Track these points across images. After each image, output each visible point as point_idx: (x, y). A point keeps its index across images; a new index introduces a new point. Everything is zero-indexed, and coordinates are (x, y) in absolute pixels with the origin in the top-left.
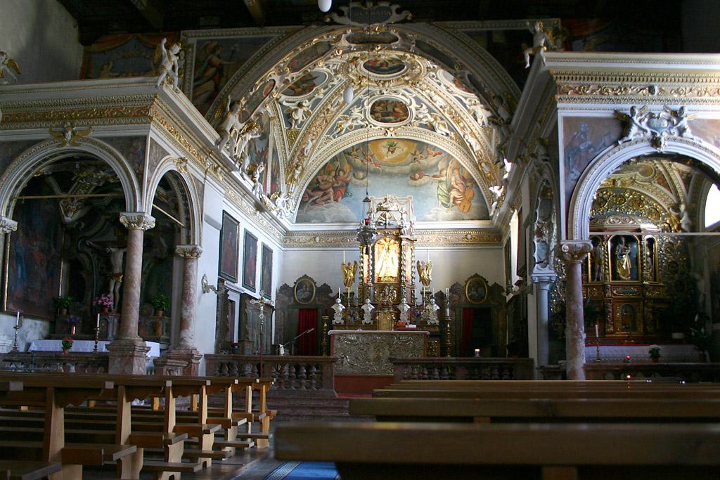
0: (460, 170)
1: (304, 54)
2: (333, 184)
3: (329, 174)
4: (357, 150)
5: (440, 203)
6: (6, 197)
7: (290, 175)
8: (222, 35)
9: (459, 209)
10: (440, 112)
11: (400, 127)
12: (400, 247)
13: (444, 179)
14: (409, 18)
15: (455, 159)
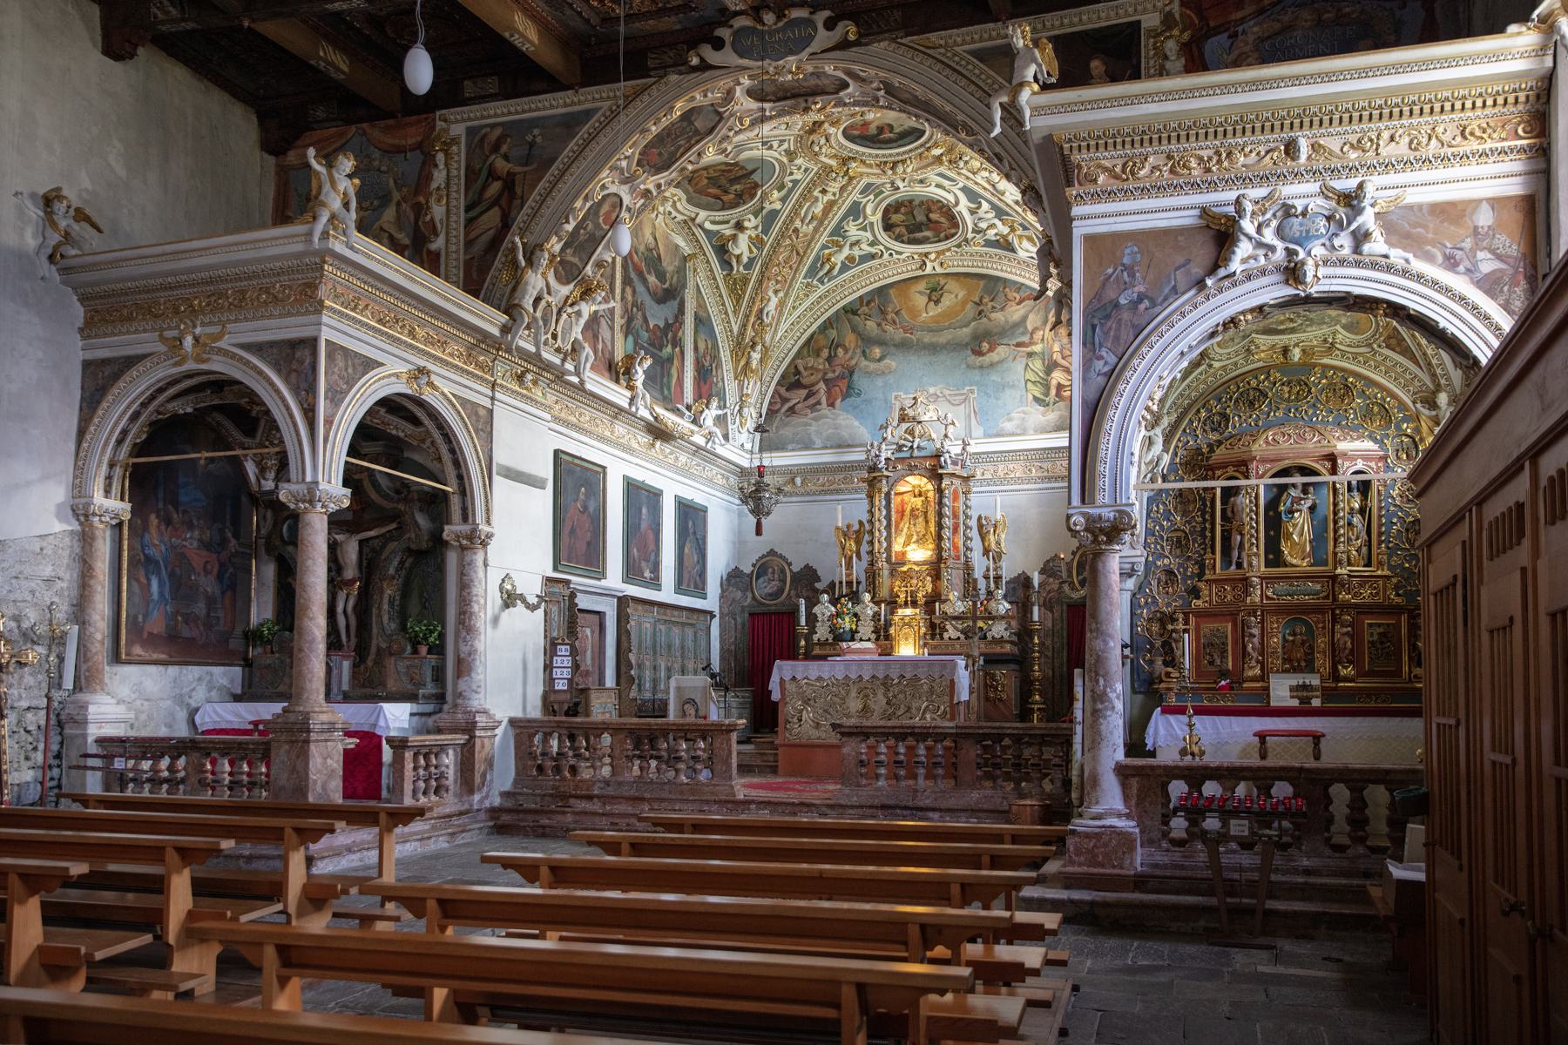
1: (669, 135)
2: (825, 374)
3: (818, 356)
5: (1031, 397)
6: (100, 462)
7: (742, 363)
8: (510, 113)
11: (949, 249)
13: (1038, 348)
14: (852, 37)
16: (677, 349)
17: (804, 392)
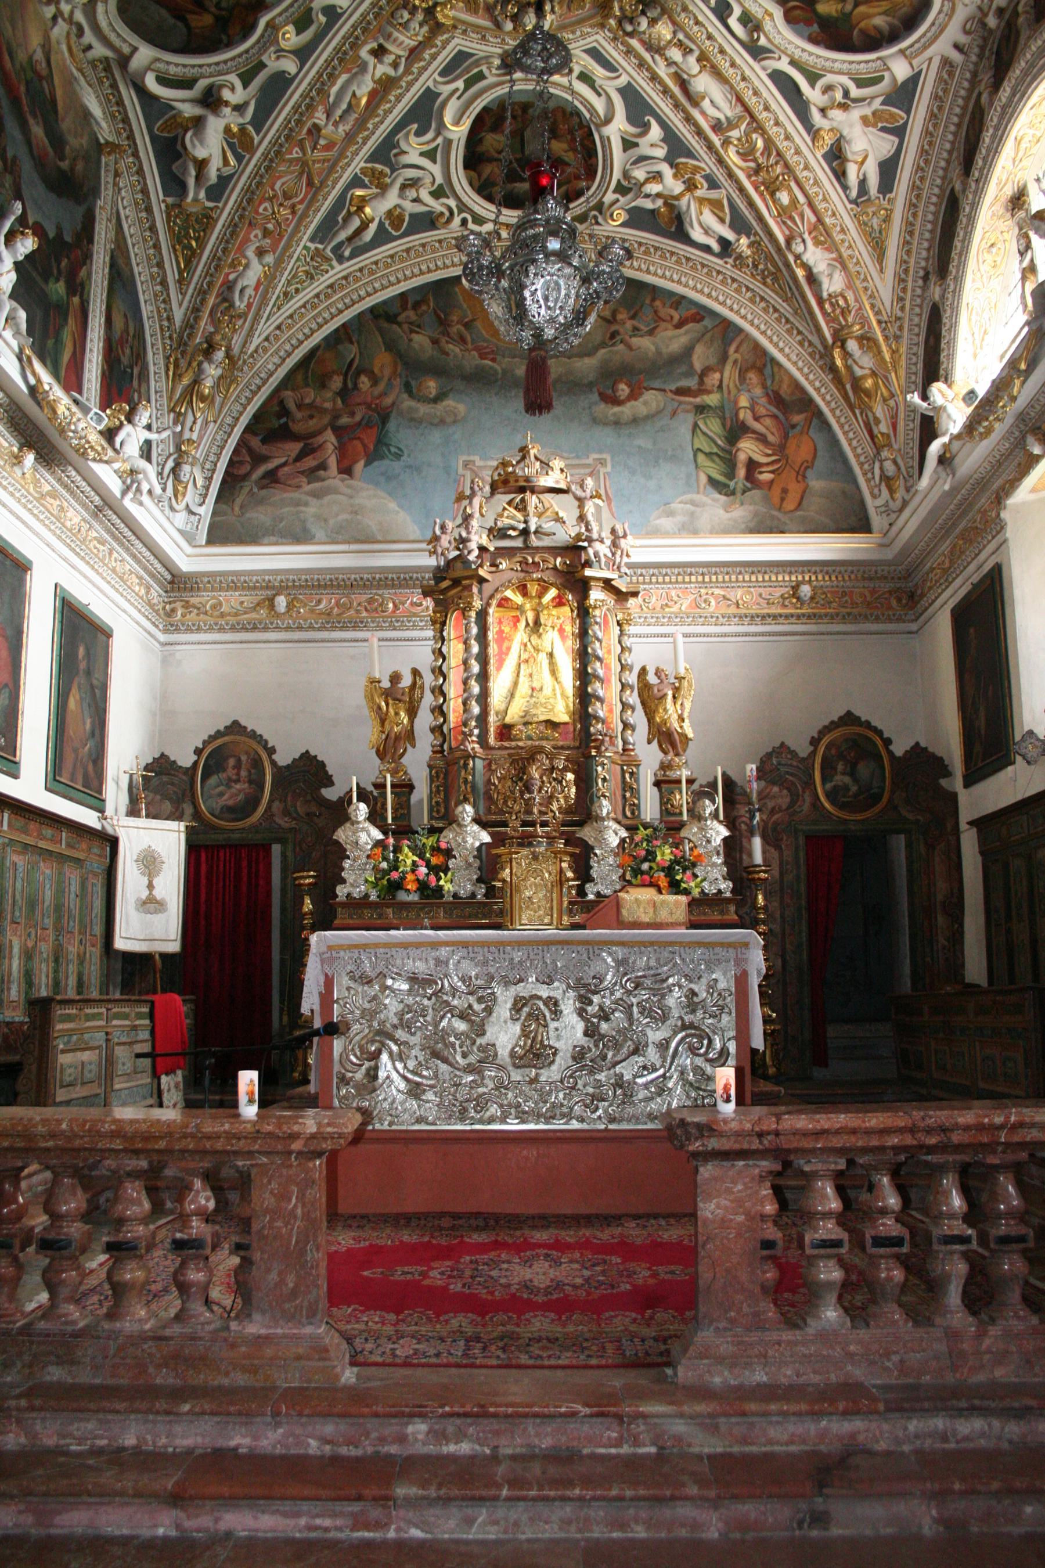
0: (768, 371)
2: (336, 417)
3: (323, 386)
4: (416, 306)
5: (703, 479)
7: (186, 381)
9: (766, 499)
10: (710, 147)
12: (583, 613)
13: (712, 399)
15: (748, 336)
16: (76, 300)
17: (295, 448)
